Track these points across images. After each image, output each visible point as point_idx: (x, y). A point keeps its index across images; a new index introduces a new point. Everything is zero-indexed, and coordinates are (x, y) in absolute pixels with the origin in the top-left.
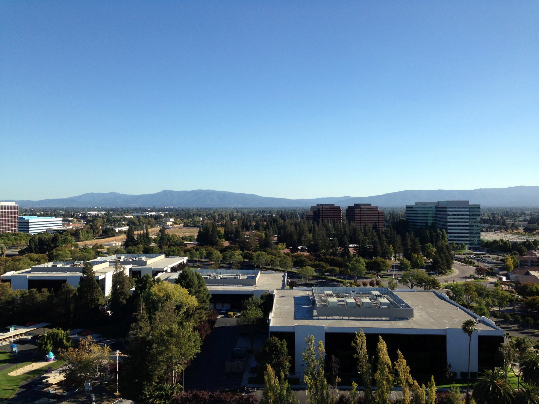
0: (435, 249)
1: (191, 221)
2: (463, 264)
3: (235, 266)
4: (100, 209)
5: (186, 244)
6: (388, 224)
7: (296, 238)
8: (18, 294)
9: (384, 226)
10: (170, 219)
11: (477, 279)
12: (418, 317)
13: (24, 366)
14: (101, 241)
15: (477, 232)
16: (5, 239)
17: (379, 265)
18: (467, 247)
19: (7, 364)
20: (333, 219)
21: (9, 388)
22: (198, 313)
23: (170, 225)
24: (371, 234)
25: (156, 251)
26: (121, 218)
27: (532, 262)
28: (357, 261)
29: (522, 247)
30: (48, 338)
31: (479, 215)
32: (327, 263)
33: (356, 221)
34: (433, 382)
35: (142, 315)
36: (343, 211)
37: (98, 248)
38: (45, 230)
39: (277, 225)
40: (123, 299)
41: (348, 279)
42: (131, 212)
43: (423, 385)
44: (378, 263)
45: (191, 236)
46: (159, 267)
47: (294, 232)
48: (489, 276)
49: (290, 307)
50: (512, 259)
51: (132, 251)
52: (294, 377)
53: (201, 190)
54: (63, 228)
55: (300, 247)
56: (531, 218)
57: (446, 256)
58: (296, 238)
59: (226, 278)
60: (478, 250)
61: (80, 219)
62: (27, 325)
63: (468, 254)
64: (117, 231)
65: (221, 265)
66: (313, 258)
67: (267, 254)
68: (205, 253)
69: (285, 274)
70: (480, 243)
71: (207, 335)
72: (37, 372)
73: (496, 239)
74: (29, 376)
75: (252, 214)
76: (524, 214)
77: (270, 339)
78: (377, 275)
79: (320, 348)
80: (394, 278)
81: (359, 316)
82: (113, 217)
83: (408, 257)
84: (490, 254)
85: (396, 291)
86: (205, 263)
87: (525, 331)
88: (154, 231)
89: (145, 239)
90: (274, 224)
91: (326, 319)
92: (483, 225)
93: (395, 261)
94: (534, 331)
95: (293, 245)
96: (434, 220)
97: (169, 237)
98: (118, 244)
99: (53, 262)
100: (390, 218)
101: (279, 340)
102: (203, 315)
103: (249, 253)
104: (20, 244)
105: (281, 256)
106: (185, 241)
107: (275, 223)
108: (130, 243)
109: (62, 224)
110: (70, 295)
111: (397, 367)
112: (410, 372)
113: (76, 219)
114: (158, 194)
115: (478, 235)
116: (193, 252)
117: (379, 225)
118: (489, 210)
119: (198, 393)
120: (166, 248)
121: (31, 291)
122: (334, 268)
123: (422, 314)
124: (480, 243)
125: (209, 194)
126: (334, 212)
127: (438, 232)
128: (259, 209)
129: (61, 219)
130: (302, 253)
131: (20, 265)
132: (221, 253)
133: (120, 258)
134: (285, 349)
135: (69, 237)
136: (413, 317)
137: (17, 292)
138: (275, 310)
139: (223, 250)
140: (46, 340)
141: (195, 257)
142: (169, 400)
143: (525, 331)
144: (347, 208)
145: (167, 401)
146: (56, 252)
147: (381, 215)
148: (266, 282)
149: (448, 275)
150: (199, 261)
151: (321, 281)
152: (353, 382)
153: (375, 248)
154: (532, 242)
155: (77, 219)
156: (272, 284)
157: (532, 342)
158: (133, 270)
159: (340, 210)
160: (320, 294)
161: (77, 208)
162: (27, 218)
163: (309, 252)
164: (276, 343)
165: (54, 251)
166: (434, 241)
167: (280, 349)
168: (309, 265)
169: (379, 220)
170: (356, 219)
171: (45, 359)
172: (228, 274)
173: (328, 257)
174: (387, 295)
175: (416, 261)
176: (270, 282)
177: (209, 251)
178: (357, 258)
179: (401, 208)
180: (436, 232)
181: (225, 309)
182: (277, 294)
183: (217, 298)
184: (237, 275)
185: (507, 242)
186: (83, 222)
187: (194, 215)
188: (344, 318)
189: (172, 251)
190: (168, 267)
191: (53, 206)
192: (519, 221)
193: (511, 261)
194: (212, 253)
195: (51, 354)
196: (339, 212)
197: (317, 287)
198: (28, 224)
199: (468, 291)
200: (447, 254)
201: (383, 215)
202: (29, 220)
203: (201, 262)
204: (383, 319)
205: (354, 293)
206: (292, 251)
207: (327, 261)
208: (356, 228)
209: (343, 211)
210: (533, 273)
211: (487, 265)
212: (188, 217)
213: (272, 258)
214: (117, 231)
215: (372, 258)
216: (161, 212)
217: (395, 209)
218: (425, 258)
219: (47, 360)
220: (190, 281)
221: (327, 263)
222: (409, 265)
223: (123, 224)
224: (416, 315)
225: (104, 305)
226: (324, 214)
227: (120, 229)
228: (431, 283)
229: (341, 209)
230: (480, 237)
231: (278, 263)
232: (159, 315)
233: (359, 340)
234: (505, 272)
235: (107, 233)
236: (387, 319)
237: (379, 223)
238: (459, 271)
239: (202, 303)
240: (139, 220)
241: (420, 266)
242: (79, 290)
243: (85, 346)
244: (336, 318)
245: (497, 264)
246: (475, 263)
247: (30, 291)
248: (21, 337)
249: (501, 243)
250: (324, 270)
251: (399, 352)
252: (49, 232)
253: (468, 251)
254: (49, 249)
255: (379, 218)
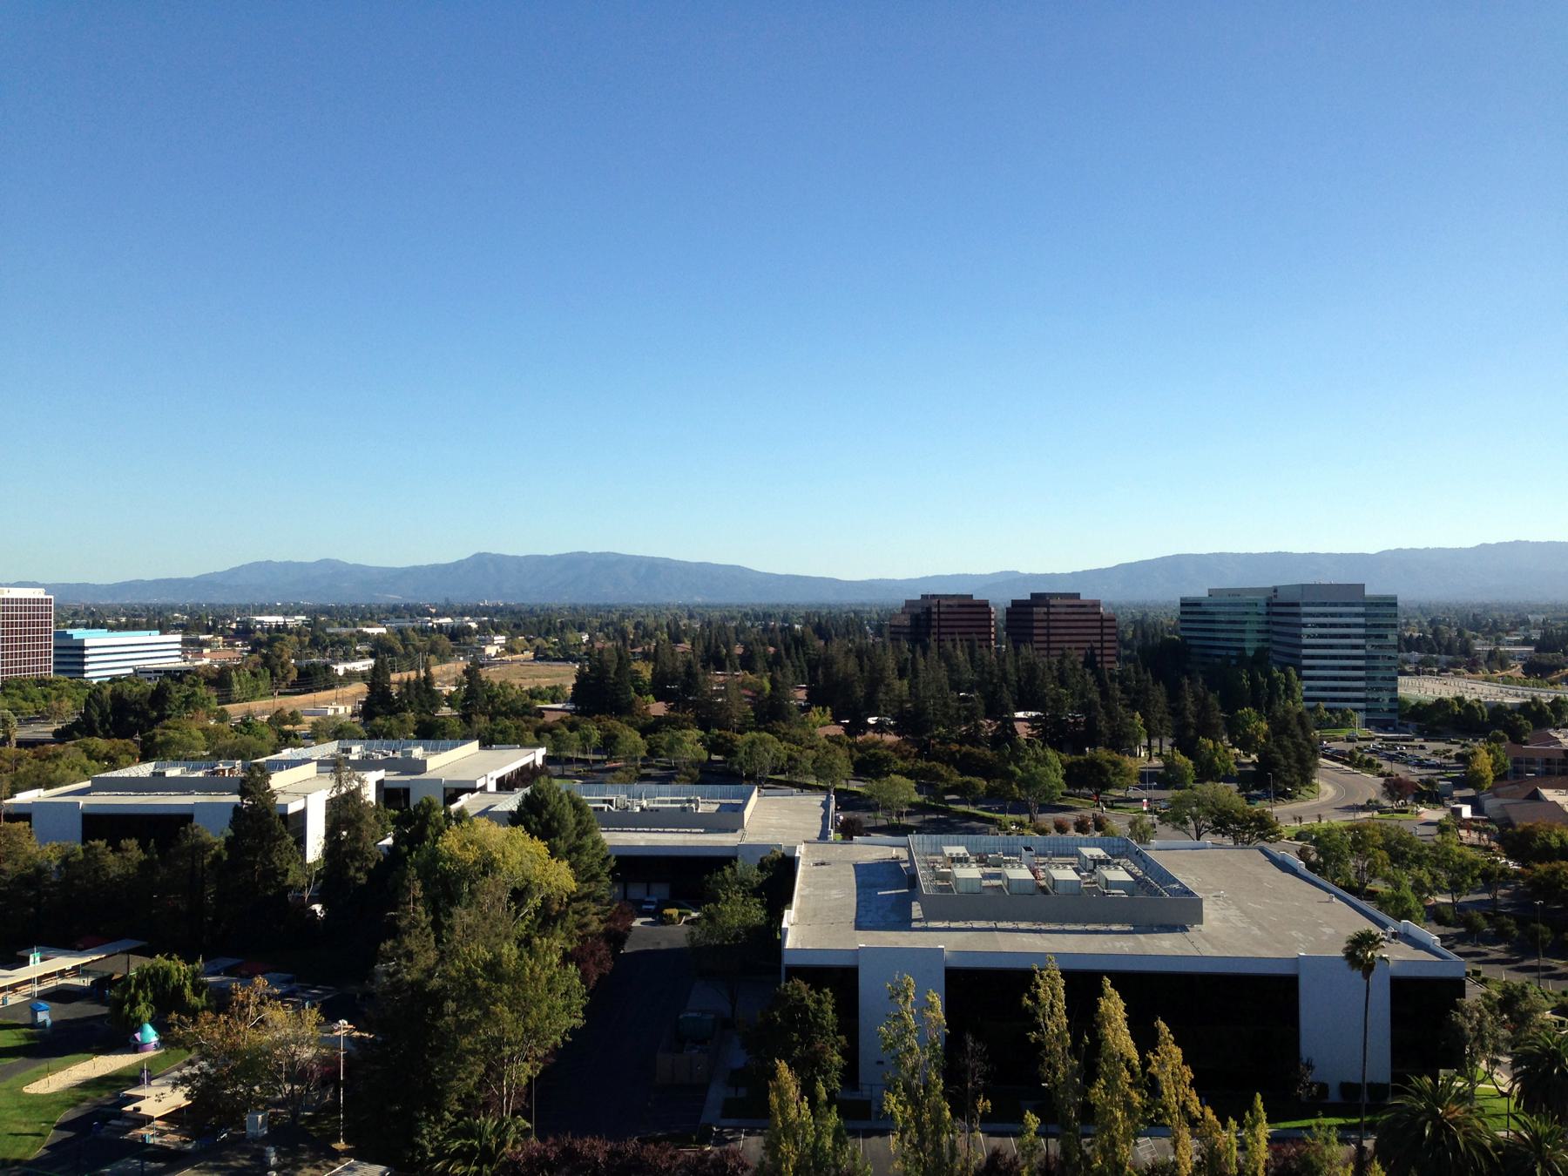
0: (1264, 726)
1: (555, 643)
2: (1346, 768)
3: (685, 774)
4: (291, 608)
5: (541, 709)
6: (1128, 652)
7: (860, 692)
8: (53, 855)
9: (1118, 659)
10: (495, 638)
11: (1388, 812)
12: (1216, 924)
13: (69, 1064)
14: (294, 703)
15: (1388, 674)
16: (14, 695)
17: (1103, 771)
18: (1359, 718)
19: (21, 1058)
20: (968, 637)
21: (27, 1130)
22: (575, 912)
23: (495, 656)
24: (1078, 682)
25: (455, 732)
26: (352, 635)
27: (1548, 761)
28: (1038, 760)
29: (1518, 719)
30: (140, 984)
31: (1394, 626)
32: (952, 767)
33: (1037, 642)
34: (1259, 1111)
35: (414, 918)
36: (998, 614)
37: (285, 722)
38: (131, 671)
39: (805, 654)
40: (358, 870)
41: (1011, 812)
42: (382, 616)
43: (1231, 1120)
44: (1100, 765)
45: (555, 687)
46: (463, 777)
47: (854, 675)
48: (1421, 803)
49: (844, 894)
50: (1489, 754)
51: (385, 730)
52: (856, 1096)
53: (586, 553)
54: (183, 664)
55: (871, 720)
56: (1546, 636)
57: (1298, 746)
58: (860, 692)
59: (657, 810)
60: (1390, 728)
61: (232, 637)
62: (80, 946)
63: (1360, 739)
64: (341, 673)
65: (644, 771)
66: (911, 752)
67: (776, 739)
68: (596, 736)
69: (828, 797)
70: (1395, 706)
71: (601, 976)
72: (109, 1083)
73: (1444, 695)
74: (84, 1093)
75: (734, 624)
76: (1525, 622)
77: (786, 987)
78: (1097, 801)
79: (930, 1014)
80: (1145, 808)
81: (1045, 921)
82: (329, 630)
83: (1188, 748)
84: (1426, 741)
85: (1151, 847)
86: (597, 767)
87: (1527, 963)
88: (448, 673)
89: (423, 694)
90: (797, 653)
91: (949, 929)
92: (1405, 655)
93: (1150, 759)
94: (1555, 963)
95: (851, 712)
96: (1263, 640)
97: (493, 691)
98: (344, 710)
99: (153, 764)
100: (1134, 635)
101: (810, 989)
102: (590, 916)
103: (725, 738)
104: (59, 709)
105: (816, 746)
106: (538, 701)
107: (800, 650)
108: (378, 709)
109: (179, 653)
110: (203, 859)
111: (1154, 1069)
112: (1193, 1084)
113: (220, 638)
114: (458, 565)
115: (1390, 685)
116: (562, 735)
117: (1102, 655)
118: (1422, 613)
119: (577, 1144)
120: (482, 722)
121: (91, 847)
122: (973, 779)
123: (1227, 913)
124: (1396, 707)
125: (608, 564)
126: (973, 616)
127: (1275, 675)
128: (752, 610)
129: (179, 638)
130: (878, 736)
131: (58, 773)
132: (643, 737)
133: (349, 751)
134: (830, 1016)
135: (202, 691)
136: (1202, 923)
137: (49, 849)
138: (801, 902)
139: (649, 728)
140: (132, 990)
141: (568, 748)
142: (490, 1165)
143: (1527, 963)
144: (1010, 605)
145: (485, 1166)
146: (163, 734)
147: (1108, 627)
148: (774, 821)
149: (1304, 801)
150: (578, 761)
151: (935, 817)
152: (1028, 1112)
153: (1091, 723)
154: (1547, 704)
155: (225, 637)
156: (791, 828)
157: (1549, 996)
158: (386, 786)
159: (990, 613)
160: (931, 854)
161: (224, 605)
162: (77, 634)
163: (898, 734)
164: (803, 999)
165: (157, 730)
166: (1264, 700)
167: (815, 1017)
168: (899, 772)
169: (1102, 641)
170: (1035, 638)
171: (130, 1044)
172: (662, 798)
173: (954, 747)
174: (1127, 857)
175: (1211, 761)
176: (787, 822)
177: (609, 730)
178: (1039, 750)
179: (1166, 607)
180: (1268, 674)
181: (654, 899)
182: (806, 855)
183: (632, 866)
184: (689, 801)
185: (1476, 705)
186: (243, 646)
187: (563, 626)
188: (1000, 925)
189: (501, 732)
190: (489, 777)
191: (155, 601)
192: (1510, 644)
193: (1486, 761)
194: (616, 737)
195: (149, 1029)
196: (986, 616)
197: (921, 836)
198: (80, 652)
199: (1361, 846)
200: (1300, 741)
201: (1114, 627)
202: (83, 640)
203: (586, 761)
204: (1115, 927)
205: (1029, 853)
206: (850, 731)
207: (950, 760)
208: (1035, 663)
209: (998, 614)
210: (1549, 794)
211: (1416, 770)
212: (548, 633)
213: (791, 750)
214: (341, 673)
215: (1083, 752)
216: (467, 618)
217: (1149, 607)
218: (1237, 750)
219: (137, 1048)
220: (552, 817)
221: (952, 767)
222: (1189, 771)
223: (359, 652)
224: (1211, 917)
225: (303, 889)
226: (942, 623)
227: (350, 666)
228: (1253, 824)
229: (993, 609)
230: (1395, 689)
231: (809, 765)
232: (462, 916)
233: (1045, 991)
234: (1470, 792)
235: (311, 679)
236: (1127, 928)
237: (1102, 648)
238: (1335, 788)
239: (588, 881)
240: (405, 640)
241: (1223, 773)
242: (230, 843)
243: (248, 1006)
244: (976, 924)
245: (1445, 768)
246: (1381, 766)
247: (87, 846)
248: (61, 982)
249: (1457, 709)
250: (942, 785)
251: (1162, 1025)
252: (143, 676)
253: (1362, 732)
254: (143, 725)
255: (1102, 634)
